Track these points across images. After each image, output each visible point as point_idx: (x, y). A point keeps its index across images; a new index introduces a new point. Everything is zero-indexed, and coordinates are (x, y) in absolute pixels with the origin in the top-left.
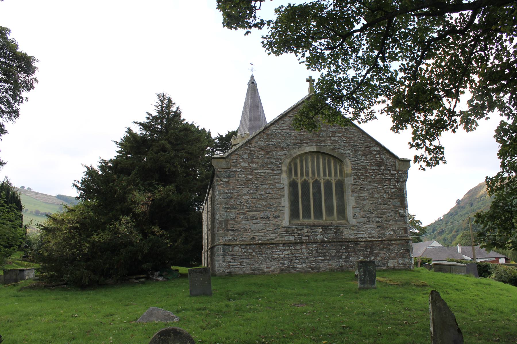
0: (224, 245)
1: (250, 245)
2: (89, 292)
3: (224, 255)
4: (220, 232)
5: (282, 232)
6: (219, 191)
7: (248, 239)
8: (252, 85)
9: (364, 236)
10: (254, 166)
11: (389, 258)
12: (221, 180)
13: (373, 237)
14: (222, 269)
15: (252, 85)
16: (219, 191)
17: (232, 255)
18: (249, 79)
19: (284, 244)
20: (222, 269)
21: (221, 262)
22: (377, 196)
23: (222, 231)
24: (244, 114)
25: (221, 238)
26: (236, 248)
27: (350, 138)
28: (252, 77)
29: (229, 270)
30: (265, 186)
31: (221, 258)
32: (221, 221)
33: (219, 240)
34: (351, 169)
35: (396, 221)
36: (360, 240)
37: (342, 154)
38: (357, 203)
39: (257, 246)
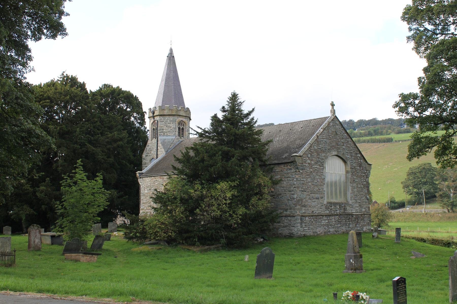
0: (302, 216)
1: (312, 216)
2: (298, 258)
3: (301, 223)
4: (297, 207)
5: (324, 208)
6: (296, 178)
7: (310, 212)
8: (171, 58)
9: (354, 211)
10: (313, 162)
11: (365, 226)
12: (299, 172)
13: (357, 212)
14: (299, 232)
15: (171, 58)
16: (296, 178)
17: (305, 223)
18: (168, 52)
19: (326, 216)
20: (299, 232)
21: (299, 227)
22: (359, 186)
23: (299, 207)
24: (162, 81)
25: (298, 211)
26: (307, 218)
27: (349, 147)
28: (171, 50)
29: (304, 233)
30: (317, 177)
31: (299, 225)
32: (299, 200)
33: (297, 212)
34: (349, 168)
35: (366, 202)
36: (354, 214)
37: (347, 158)
38: (352, 190)
39: (315, 217)
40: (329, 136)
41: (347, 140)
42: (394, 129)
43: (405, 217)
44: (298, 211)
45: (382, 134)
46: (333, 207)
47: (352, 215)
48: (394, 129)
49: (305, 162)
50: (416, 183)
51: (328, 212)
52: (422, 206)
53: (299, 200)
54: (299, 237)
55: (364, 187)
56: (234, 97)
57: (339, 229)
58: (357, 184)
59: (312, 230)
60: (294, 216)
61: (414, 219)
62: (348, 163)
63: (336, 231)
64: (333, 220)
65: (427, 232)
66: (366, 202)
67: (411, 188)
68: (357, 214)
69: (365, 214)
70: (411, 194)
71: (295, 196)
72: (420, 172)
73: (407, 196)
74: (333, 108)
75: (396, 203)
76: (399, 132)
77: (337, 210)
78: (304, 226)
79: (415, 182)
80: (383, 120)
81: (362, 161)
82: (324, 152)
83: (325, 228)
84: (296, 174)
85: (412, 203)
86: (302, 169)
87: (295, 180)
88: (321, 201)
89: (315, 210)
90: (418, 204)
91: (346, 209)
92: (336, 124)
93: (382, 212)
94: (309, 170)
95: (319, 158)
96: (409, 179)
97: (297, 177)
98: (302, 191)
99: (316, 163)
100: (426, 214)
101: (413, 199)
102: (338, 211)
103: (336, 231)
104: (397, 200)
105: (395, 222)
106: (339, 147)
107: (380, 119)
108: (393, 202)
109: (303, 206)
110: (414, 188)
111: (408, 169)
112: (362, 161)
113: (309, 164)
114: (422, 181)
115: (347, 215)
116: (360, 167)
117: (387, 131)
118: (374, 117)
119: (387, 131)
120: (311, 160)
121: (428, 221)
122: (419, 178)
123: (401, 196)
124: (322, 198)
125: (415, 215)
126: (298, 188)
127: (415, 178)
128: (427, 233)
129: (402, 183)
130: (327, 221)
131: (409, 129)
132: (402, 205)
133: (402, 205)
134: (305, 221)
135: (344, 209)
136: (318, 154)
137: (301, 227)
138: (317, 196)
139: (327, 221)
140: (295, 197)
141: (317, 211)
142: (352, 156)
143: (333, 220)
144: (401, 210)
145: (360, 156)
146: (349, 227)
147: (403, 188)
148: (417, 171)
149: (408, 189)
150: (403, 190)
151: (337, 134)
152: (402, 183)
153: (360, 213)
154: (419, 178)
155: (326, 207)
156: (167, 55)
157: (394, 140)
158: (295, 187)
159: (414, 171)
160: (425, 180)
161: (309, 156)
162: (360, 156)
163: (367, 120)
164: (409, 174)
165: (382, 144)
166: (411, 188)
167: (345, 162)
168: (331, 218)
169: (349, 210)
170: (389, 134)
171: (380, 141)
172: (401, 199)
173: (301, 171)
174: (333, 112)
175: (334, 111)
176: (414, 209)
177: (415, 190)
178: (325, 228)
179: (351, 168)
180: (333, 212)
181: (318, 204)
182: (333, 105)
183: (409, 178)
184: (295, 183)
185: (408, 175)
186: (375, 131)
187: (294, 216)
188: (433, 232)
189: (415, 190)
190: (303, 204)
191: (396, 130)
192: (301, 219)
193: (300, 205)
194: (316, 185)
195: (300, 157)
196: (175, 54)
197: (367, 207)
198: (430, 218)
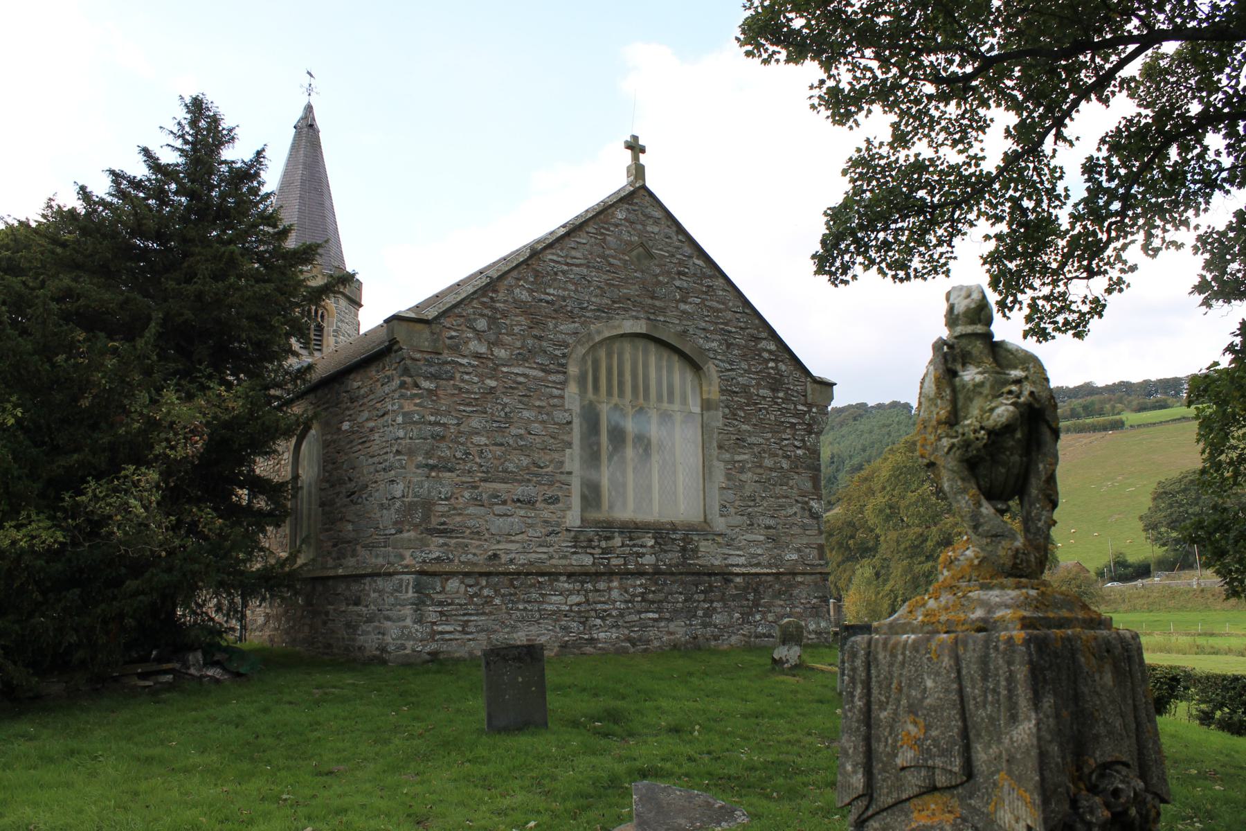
0: (422, 573)
1: (488, 574)
3: (419, 604)
4: (405, 535)
7: (481, 559)
9: (742, 560)
10: (502, 353)
12: (417, 386)
14: (410, 644)
16: (405, 415)
17: (441, 604)
18: (299, 113)
19: (570, 575)
20: (410, 644)
21: (408, 622)
22: (768, 463)
23: (412, 534)
25: (407, 553)
26: (453, 584)
29: (433, 646)
30: (526, 414)
31: (408, 611)
33: (402, 557)
34: (715, 388)
35: (804, 527)
36: (737, 570)
37: (702, 351)
38: (729, 477)
39: (505, 580)
40: (605, 257)
41: (707, 282)
42: (1130, 402)
43: (1150, 600)
44: (407, 553)
45: (1101, 413)
46: (617, 541)
47: (726, 576)
48: (1130, 402)
49: (455, 349)
50: (1174, 517)
51: (588, 560)
52: (1192, 572)
53: (411, 507)
54: (408, 664)
55: (795, 468)
56: (197, 107)
57: (652, 633)
58: (759, 455)
59: (483, 636)
60: (390, 575)
61: (1171, 604)
62: (711, 369)
63: (629, 639)
64: (615, 594)
65: (1188, 634)
66: (804, 527)
67: (1163, 529)
68: (754, 570)
69: (795, 574)
70: (1164, 545)
71: (398, 490)
72: (1184, 491)
73: (1156, 548)
74: (636, 158)
75: (1130, 566)
76: (1142, 409)
77: (642, 555)
78: (433, 617)
79: (1171, 514)
80: (1107, 386)
81: (783, 367)
82: (571, 316)
83: (566, 629)
84: (402, 396)
85: (1167, 565)
86: (434, 377)
87: (400, 419)
88: (546, 514)
89: (508, 552)
90: (1182, 568)
91: (695, 550)
92: (649, 217)
93: (1079, 587)
94: (473, 383)
95: (540, 338)
96: (1157, 509)
97: (408, 406)
98: (433, 468)
99: (523, 357)
100: (1202, 591)
101: (1171, 556)
102: (649, 560)
103: (629, 639)
104: (1132, 558)
105: (1126, 612)
106: (657, 303)
107: (1100, 382)
108: (1120, 563)
109: (431, 532)
110: (1173, 529)
111: (1155, 485)
112: (783, 367)
113: (478, 356)
114: (1190, 511)
115: (698, 574)
116: (774, 390)
117: (1113, 407)
118: (1088, 381)
119: (1113, 407)
120: (497, 343)
121: (1207, 608)
122: (1182, 505)
123: (1142, 549)
124: (554, 500)
125: (1174, 594)
126: (411, 452)
127: (1171, 506)
128: (1189, 639)
129: (1141, 518)
130: (575, 599)
131: (1165, 400)
132: (1143, 571)
133: (1143, 571)
134: (441, 597)
135: (684, 549)
136: (535, 323)
137: (419, 621)
138: (519, 490)
139: (575, 599)
140: (398, 494)
141: (514, 554)
142: (729, 346)
143: (615, 594)
144: (1139, 583)
145: (773, 347)
146: (705, 625)
147: (1145, 530)
148: (1176, 487)
149: (1155, 533)
150: (1144, 534)
151: (651, 256)
152: (1141, 518)
153: (770, 566)
154: (1182, 505)
155: (575, 539)
156: (295, 123)
157: (1127, 424)
158: (398, 452)
159: (1168, 489)
160: (1197, 509)
161: (482, 324)
162: (773, 347)
163: (1071, 386)
164: (1157, 497)
165: (1099, 435)
166: (1163, 529)
167: (695, 365)
168: (602, 585)
169: (710, 554)
170: (1119, 413)
171: (1094, 428)
172: (1142, 557)
173: (426, 384)
174: (638, 171)
175: (642, 167)
176: (1174, 579)
177: (1174, 534)
178: (566, 629)
179: (722, 392)
180: (614, 562)
181: (530, 526)
182: (635, 147)
183: (1157, 507)
184: (401, 433)
185: (1154, 499)
186: (1085, 408)
187: (390, 575)
188: (1212, 635)
189: (1174, 534)
190: (434, 522)
191: (1135, 403)
192: (418, 588)
193: (416, 526)
194: (521, 448)
195: (419, 326)
196: (320, 122)
197: (808, 546)
198: (1211, 599)
